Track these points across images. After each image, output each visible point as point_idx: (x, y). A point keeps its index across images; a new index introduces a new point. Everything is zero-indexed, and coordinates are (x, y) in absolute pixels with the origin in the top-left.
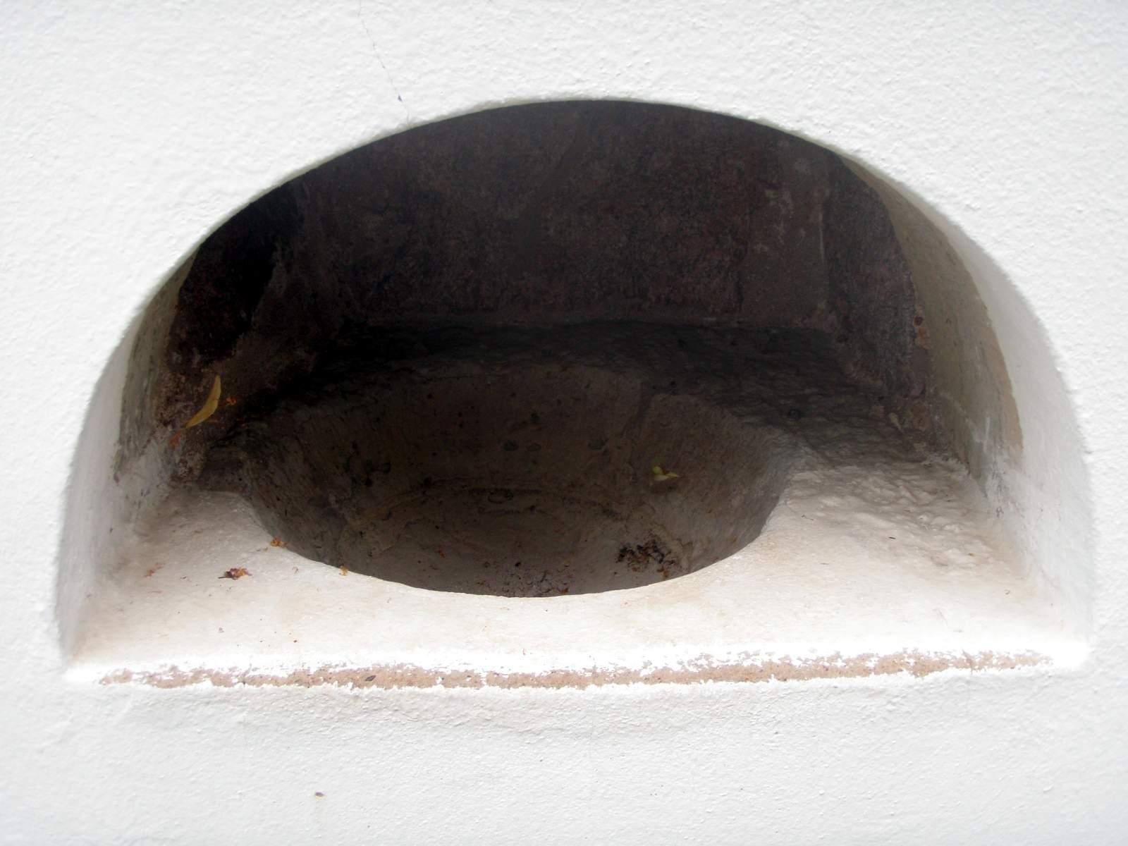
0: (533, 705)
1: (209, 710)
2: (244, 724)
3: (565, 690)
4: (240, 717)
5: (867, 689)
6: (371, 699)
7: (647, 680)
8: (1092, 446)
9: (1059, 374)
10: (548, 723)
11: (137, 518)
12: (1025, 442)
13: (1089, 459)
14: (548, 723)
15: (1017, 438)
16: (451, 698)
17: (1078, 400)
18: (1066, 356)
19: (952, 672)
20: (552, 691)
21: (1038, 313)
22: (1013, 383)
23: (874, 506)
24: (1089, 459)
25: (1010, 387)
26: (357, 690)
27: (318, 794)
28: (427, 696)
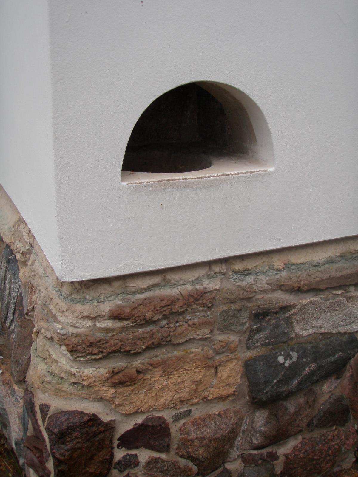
0: (196, 182)
1: (146, 188)
2: (150, 190)
3: (201, 179)
4: (150, 189)
5: (244, 176)
6: (171, 183)
7: (212, 177)
8: (272, 133)
9: (266, 121)
10: (198, 186)
11: (55, 390)
12: (257, 140)
13: (271, 135)
14: (198, 186)
15: (256, 140)
16: (184, 182)
17: (269, 125)
18: (267, 118)
19: (256, 173)
20: (199, 179)
21: (263, 111)
22: (255, 130)
23: (232, 160)
24: (271, 135)
25: (254, 131)
26: (169, 182)
27: (161, 204)
28: (180, 182)
